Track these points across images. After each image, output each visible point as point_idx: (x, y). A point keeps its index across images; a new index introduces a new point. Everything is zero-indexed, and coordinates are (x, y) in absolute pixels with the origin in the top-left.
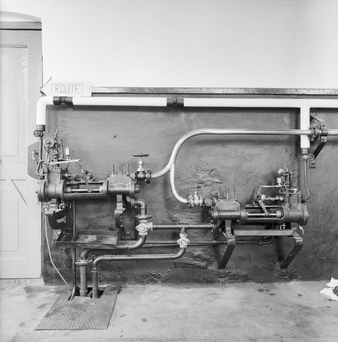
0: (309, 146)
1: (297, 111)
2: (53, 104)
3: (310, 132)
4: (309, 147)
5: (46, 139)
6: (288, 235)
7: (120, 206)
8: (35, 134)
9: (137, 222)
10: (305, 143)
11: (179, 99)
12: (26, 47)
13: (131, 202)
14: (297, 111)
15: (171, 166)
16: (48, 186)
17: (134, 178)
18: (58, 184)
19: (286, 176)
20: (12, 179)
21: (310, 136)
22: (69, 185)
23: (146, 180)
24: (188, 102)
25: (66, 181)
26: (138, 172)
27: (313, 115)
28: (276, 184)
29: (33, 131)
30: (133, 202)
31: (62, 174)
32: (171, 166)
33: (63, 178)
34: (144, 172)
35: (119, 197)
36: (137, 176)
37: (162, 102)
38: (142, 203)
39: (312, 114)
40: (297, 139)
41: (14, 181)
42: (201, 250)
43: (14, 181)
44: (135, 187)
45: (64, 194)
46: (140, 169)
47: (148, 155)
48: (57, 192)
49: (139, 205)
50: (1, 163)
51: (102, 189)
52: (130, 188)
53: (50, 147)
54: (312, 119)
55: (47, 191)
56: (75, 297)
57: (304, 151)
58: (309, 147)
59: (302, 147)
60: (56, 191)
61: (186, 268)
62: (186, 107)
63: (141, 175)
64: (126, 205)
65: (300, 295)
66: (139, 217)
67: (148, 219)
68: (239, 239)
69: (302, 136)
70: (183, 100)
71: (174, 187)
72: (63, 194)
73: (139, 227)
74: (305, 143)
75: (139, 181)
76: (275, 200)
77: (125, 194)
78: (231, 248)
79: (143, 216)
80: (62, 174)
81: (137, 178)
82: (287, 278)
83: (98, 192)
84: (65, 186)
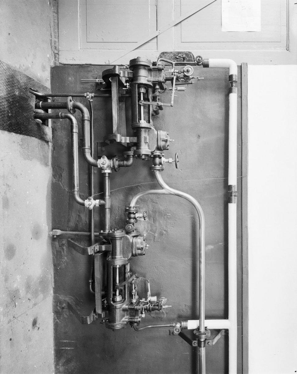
0: (189, 328)
1: (225, 316)
2: (230, 74)
3: (202, 330)
4: (188, 329)
5: (193, 69)
6: (96, 309)
7: (126, 140)
8: (200, 57)
9: (110, 157)
10: (192, 325)
11: (234, 199)
12: (288, 49)
13: (131, 151)
14: (225, 316)
15: (167, 189)
16: (145, 69)
17: (155, 154)
18: (147, 78)
19: (157, 307)
20: (158, 37)
21: (198, 329)
22: (147, 91)
23: (153, 166)
24: (233, 208)
25: (151, 87)
26: (160, 158)
27: (223, 333)
28: (152, 295)
29: (202, 56)
30: (131, 153)
31: (157, 83)
32: (167, 189)
33: (155, 83)
34: (160, 164)
35: (135, 140)
36: (156, 157)
37: (233, 180)
38: (131, 161)
39: (224, 331)
40: (195, 316)
41: (156, 39)
42: (86, 221)
43: (156, 39)
44: (145, 155)
45: (137, 85)
46: (163, 159)
47: (177, 167)
48: (139, 78)
49: (127, 159)
50: (175, 26)
51: (143, 123)
52: (145, 150)
53: (185, 73)
54: (218, 331)
55: (141, 67)
56: (35, 96)
57: (184, 324)
58: (188, 329)
59: (189, 321)
60: (141, 77)
61: (68, 207)
62: (228, 205)
63: (157, 160)
64: (128, 147)
65: (35, 323)
66: (115, 160)
67: (113, 169)
68: (91, 260)
69: (198, 321)
70: (235, 203)
71: (184, 195)
72: (136, 84)
73: (105, 159)
74: (192, 325)
75: (151, 160)
76: (133, 295)
77: (137, 145)
78: (84, 252)
79: (117, 163)
80: (157, 83)
81: (155, 157)
82: (57, 309)
83: (140, 119)
84: (146, 86)
